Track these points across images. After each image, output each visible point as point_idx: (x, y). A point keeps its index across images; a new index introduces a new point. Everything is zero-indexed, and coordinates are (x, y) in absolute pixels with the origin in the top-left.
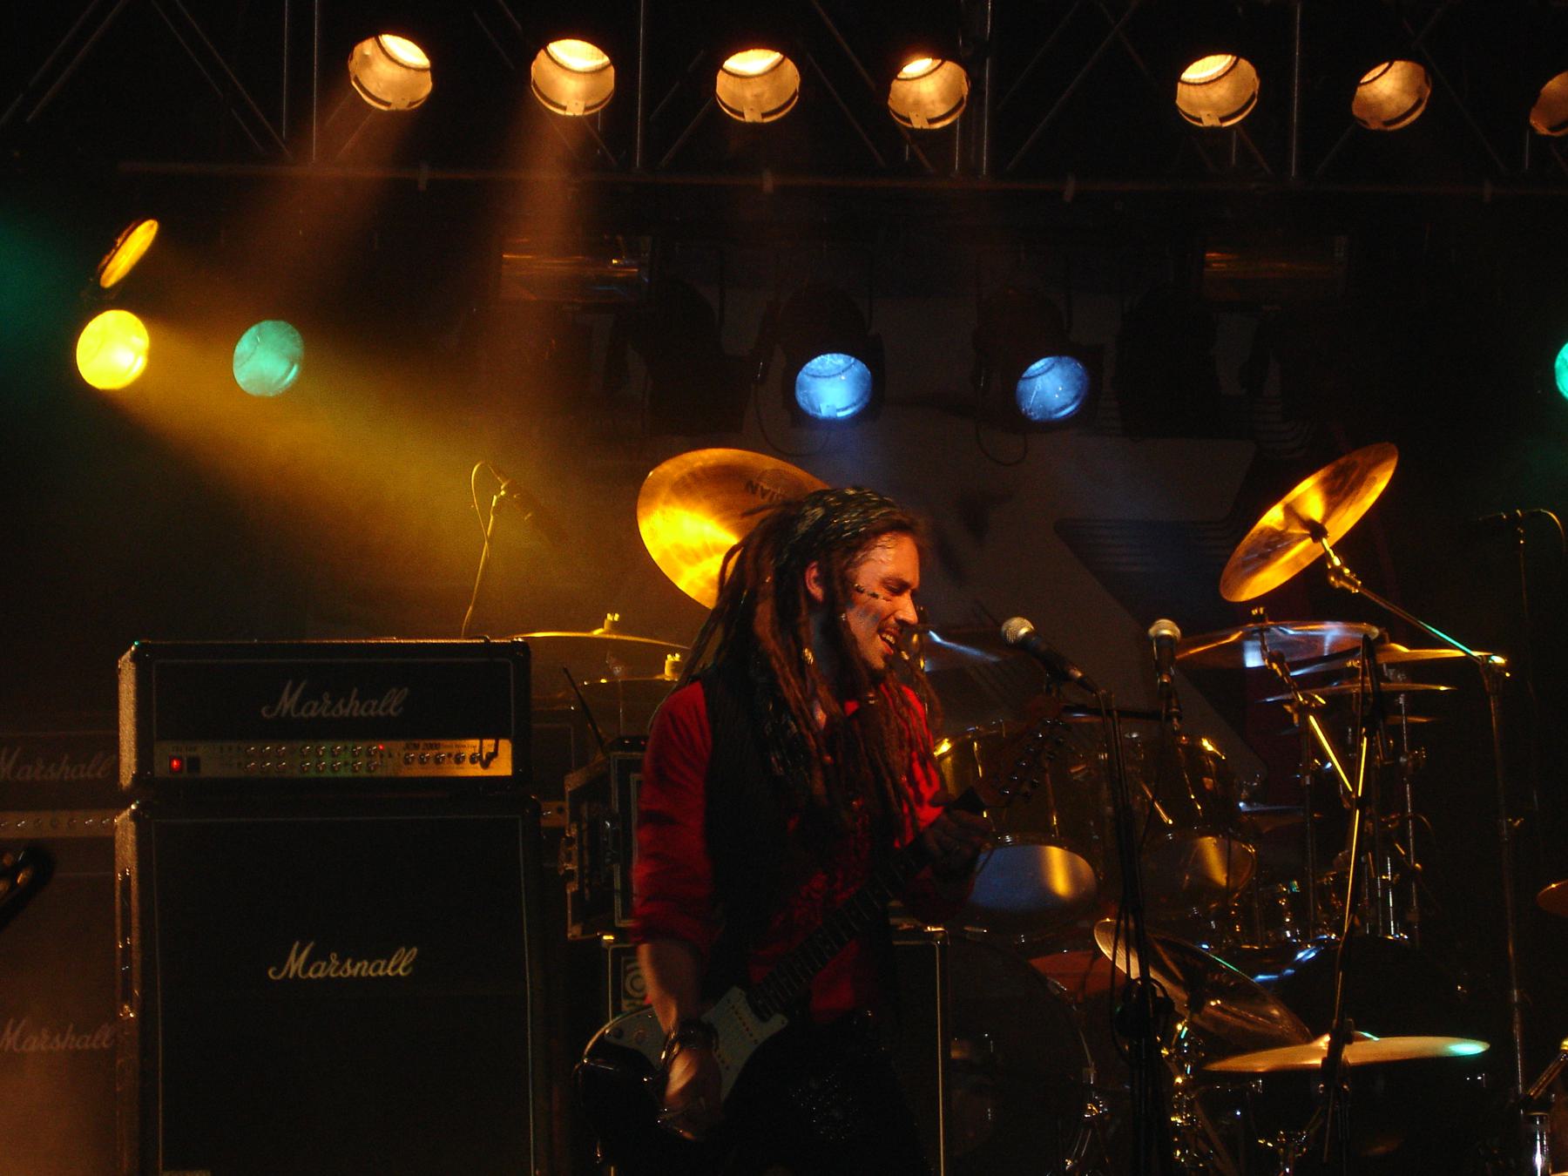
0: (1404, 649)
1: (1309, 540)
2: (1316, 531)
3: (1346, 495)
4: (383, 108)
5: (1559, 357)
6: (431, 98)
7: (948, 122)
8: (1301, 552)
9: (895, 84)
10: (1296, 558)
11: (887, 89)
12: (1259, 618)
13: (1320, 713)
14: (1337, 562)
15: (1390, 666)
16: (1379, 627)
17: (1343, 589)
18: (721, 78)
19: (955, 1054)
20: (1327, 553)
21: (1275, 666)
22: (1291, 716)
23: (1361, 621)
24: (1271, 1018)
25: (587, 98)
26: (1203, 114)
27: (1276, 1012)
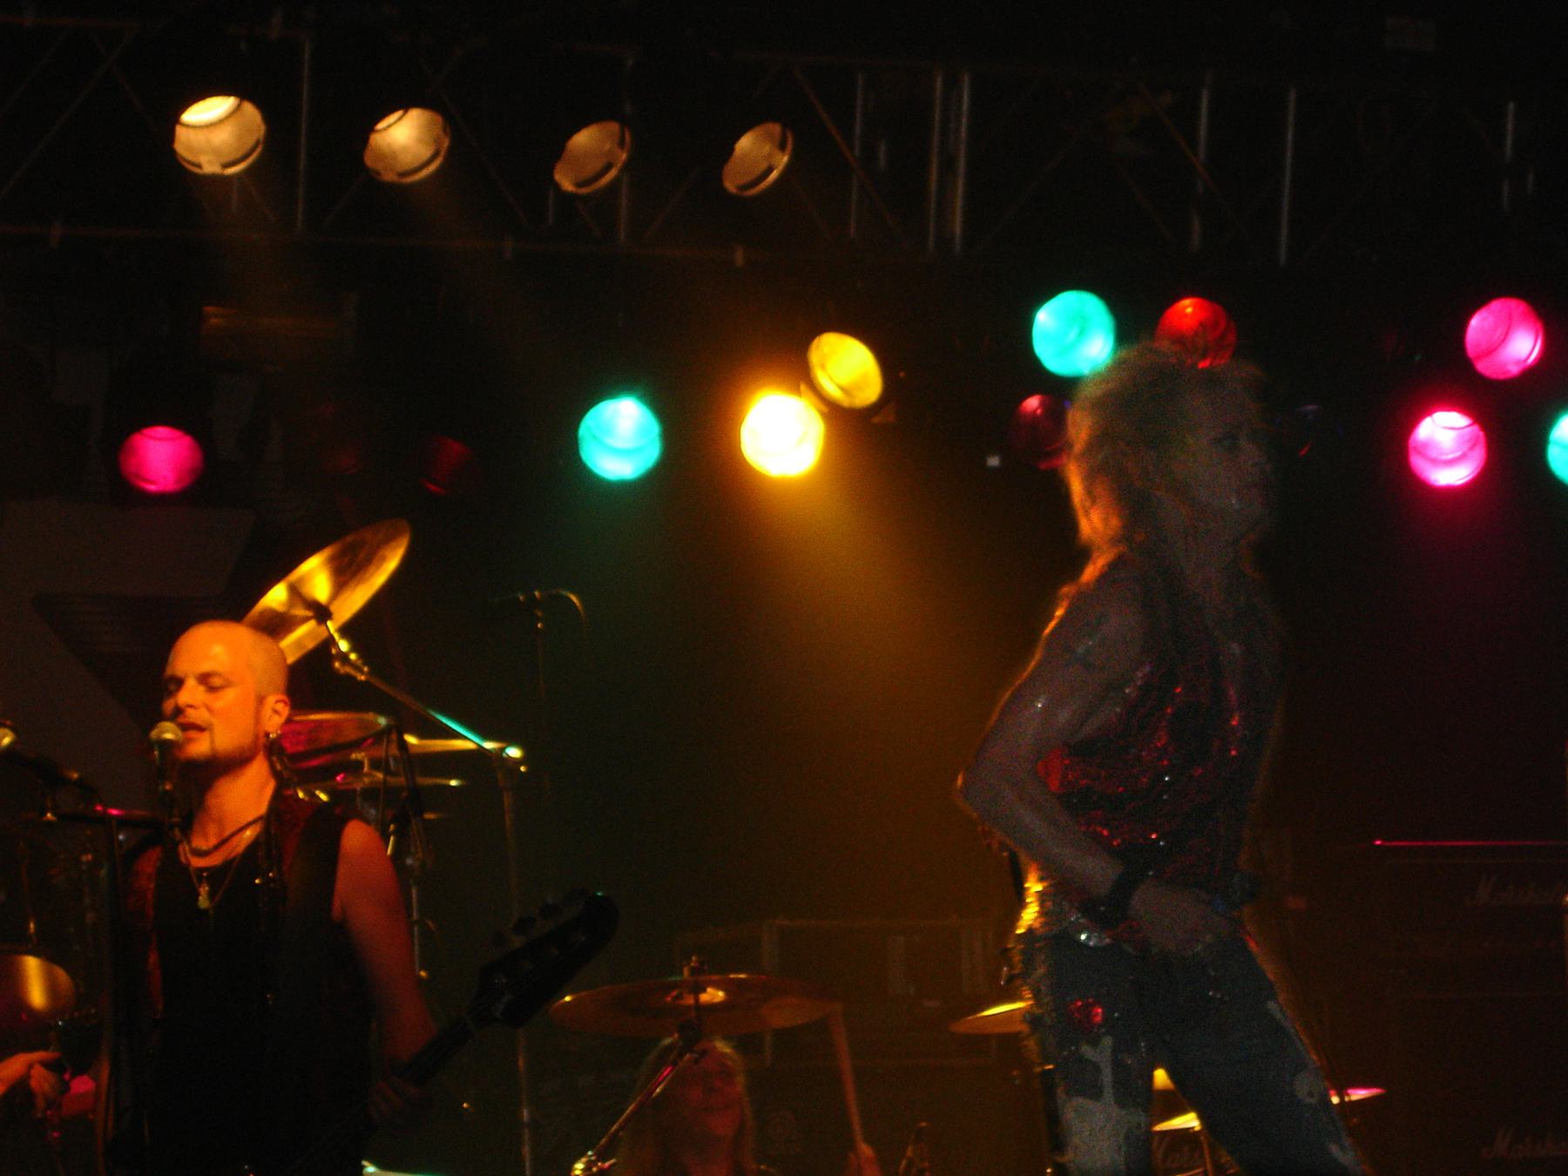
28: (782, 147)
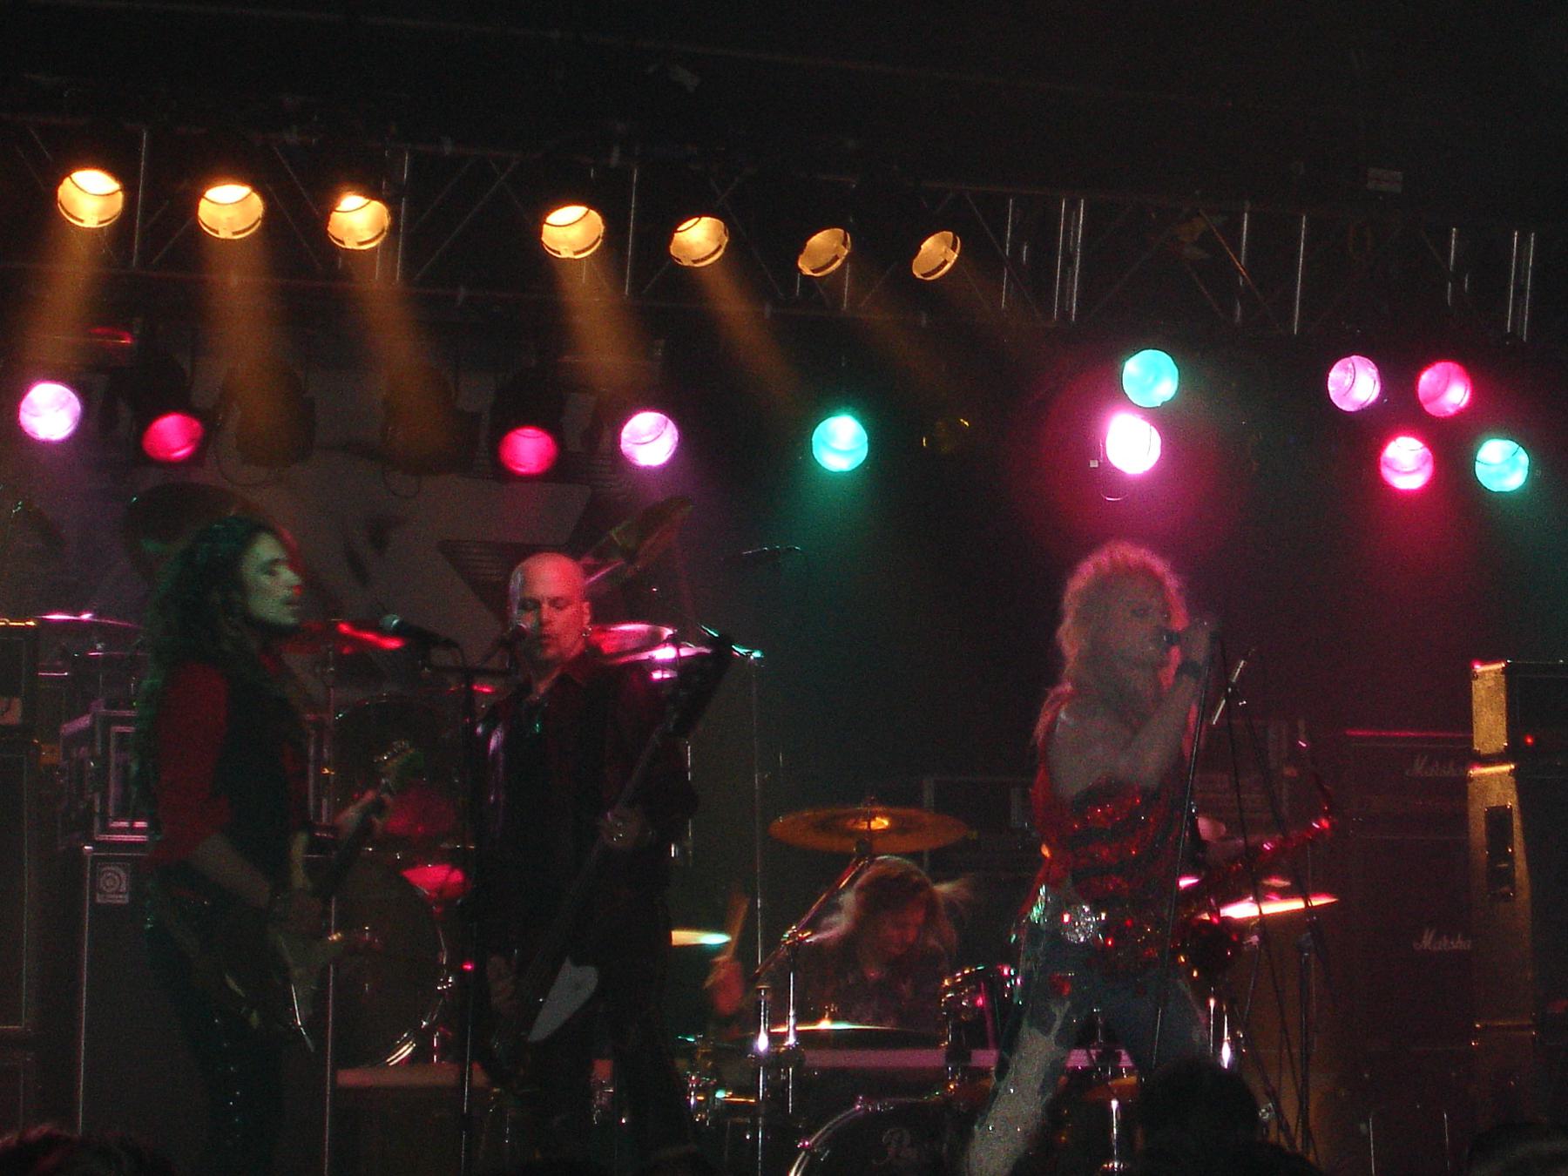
4: (838, 263)
6: (797, 259)
7: (373, 245)
9: (335, 215)
11: (326, 218)
18: (203, 204)
25: (100, 214)
26: (561, 248)
28: (954, 249)
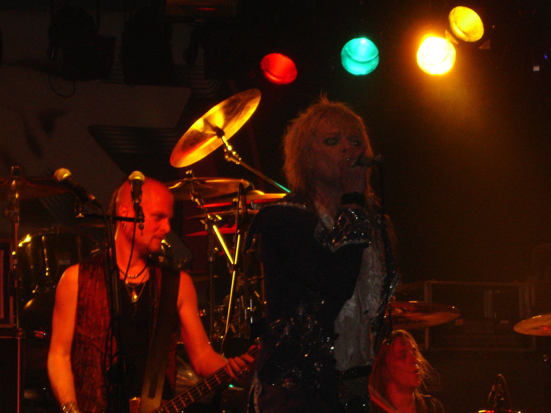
0: (261, 193)
1: (216, 137)
2: (220, 133)
3: (235, 114)
5: (343, 49)
8: (211, 144)
10: (209, 146)
12: (190, 176)
13: (220, 225)
14: (230, 148)
15: (253, 201)
16: (249, 181)
17: (231, 162)
19: (27, 395)
20: (224, 144)
21: (196, 200)
22: (204, 225)
23: (240, 178)
24: (188, 377)
27: (190, 374)
